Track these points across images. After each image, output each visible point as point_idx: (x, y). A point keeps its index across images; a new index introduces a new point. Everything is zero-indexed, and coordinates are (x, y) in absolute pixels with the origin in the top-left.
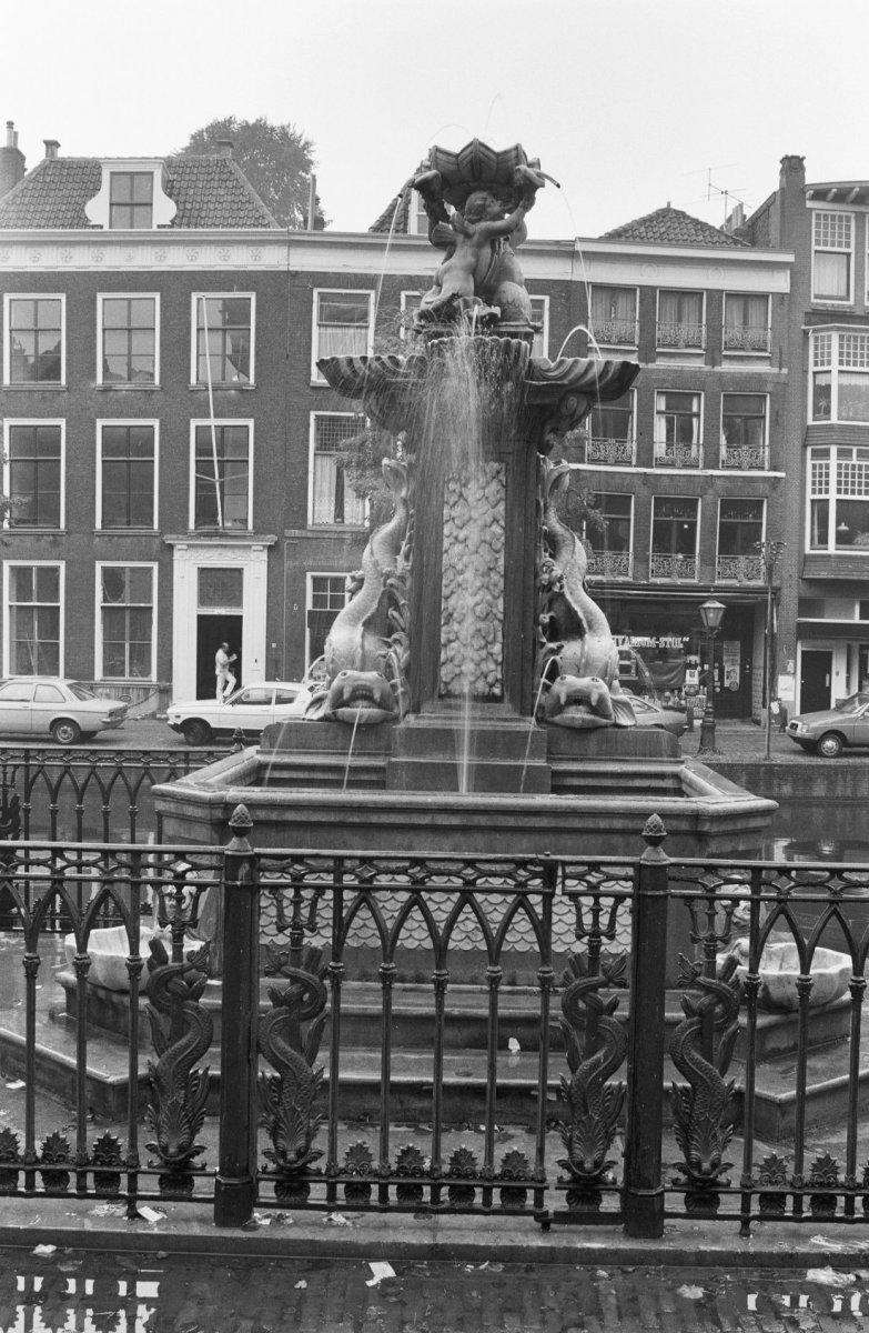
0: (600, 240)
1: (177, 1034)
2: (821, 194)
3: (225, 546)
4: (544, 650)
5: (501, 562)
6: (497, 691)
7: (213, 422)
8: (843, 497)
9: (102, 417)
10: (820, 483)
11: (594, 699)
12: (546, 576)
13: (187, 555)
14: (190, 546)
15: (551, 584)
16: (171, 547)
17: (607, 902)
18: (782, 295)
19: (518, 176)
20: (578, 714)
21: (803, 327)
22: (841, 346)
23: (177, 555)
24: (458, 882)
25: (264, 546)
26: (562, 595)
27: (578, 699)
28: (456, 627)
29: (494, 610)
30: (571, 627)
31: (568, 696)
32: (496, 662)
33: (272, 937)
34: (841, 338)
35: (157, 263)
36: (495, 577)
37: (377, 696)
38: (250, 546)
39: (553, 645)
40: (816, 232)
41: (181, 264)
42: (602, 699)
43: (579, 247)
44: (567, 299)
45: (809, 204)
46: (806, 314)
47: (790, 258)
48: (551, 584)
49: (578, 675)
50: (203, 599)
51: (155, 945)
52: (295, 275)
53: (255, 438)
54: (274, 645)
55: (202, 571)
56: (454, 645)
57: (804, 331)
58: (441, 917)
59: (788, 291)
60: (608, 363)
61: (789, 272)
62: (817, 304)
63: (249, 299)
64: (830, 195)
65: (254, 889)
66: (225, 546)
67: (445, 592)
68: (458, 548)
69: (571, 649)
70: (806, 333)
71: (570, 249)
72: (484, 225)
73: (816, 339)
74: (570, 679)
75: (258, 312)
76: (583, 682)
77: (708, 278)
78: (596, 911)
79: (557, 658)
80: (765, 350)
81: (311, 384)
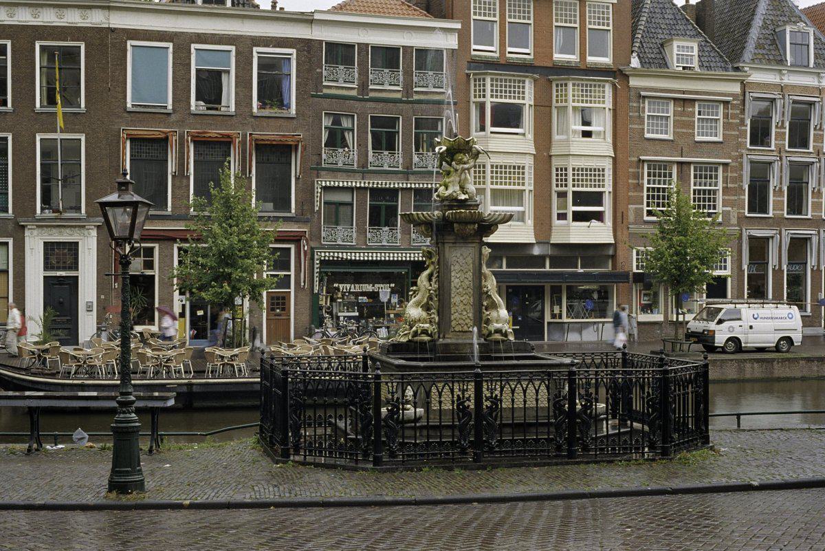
0: (328, 12)
1: (463, 417)
3: (64, 226)
4: (485, 315)
5: (472, 284)
7: (58, 136)
8: (495, 187)
10: (479, 178)
11: (504, 331)
12: (485, 289)
13: (35, 232)
14: (38, 226)
15: (487, 292)
16: (23, 227)
17: (395, 384)
18: (453, 50)
19: (474, 149)
20: (498, 337)
21: (467, 71)
22: (492, 85)
23: (27, 233)
24: (600, 357)
25: (94, 226)
26: (490, 296)
27: (498, 331)
28: (457, 308)
30: (494, 306)
31: (495, 330)
32: (471, 320)
33: (486, 393)
34: (492, 80)
35: (8, 19)
36: (470, 290)
37: (430, 332)
38: (85, 226)
39: (488, 313)
40: (474, 6)
41: (28, 19)
42: (506, 331)
43: (317, 17)
44: (309, 52)
46: (468, 62)
47: (459, 26)
48: (487, 292)
49: (67, 354)
50: (47, 266)
51: (458, 396)
52: (113, 30)
53: (86, 148)
54: (103, 297)
55: (45, 243)
56: (457, 314)
57: (467, 74)
58: (513, 386)
59: (457, 48)
60: (505, 215)
61: (457, 34)
62: (476, 56)
63: (80, 47)
65: (482, 381)
66: (64, 226)
67: (453, 295)
68: (457, 280)
69: (494, 314)
70: (468, 75)
71: (311, 18)
72: (461, 166)
73: (475, 80)
74: (495, 324)
75: (86, 57)
76: (499, 326)
77: (404, 38)
78: (393, 387)
79: (489, 317)
80: (442, 88)
81: (128, 110)
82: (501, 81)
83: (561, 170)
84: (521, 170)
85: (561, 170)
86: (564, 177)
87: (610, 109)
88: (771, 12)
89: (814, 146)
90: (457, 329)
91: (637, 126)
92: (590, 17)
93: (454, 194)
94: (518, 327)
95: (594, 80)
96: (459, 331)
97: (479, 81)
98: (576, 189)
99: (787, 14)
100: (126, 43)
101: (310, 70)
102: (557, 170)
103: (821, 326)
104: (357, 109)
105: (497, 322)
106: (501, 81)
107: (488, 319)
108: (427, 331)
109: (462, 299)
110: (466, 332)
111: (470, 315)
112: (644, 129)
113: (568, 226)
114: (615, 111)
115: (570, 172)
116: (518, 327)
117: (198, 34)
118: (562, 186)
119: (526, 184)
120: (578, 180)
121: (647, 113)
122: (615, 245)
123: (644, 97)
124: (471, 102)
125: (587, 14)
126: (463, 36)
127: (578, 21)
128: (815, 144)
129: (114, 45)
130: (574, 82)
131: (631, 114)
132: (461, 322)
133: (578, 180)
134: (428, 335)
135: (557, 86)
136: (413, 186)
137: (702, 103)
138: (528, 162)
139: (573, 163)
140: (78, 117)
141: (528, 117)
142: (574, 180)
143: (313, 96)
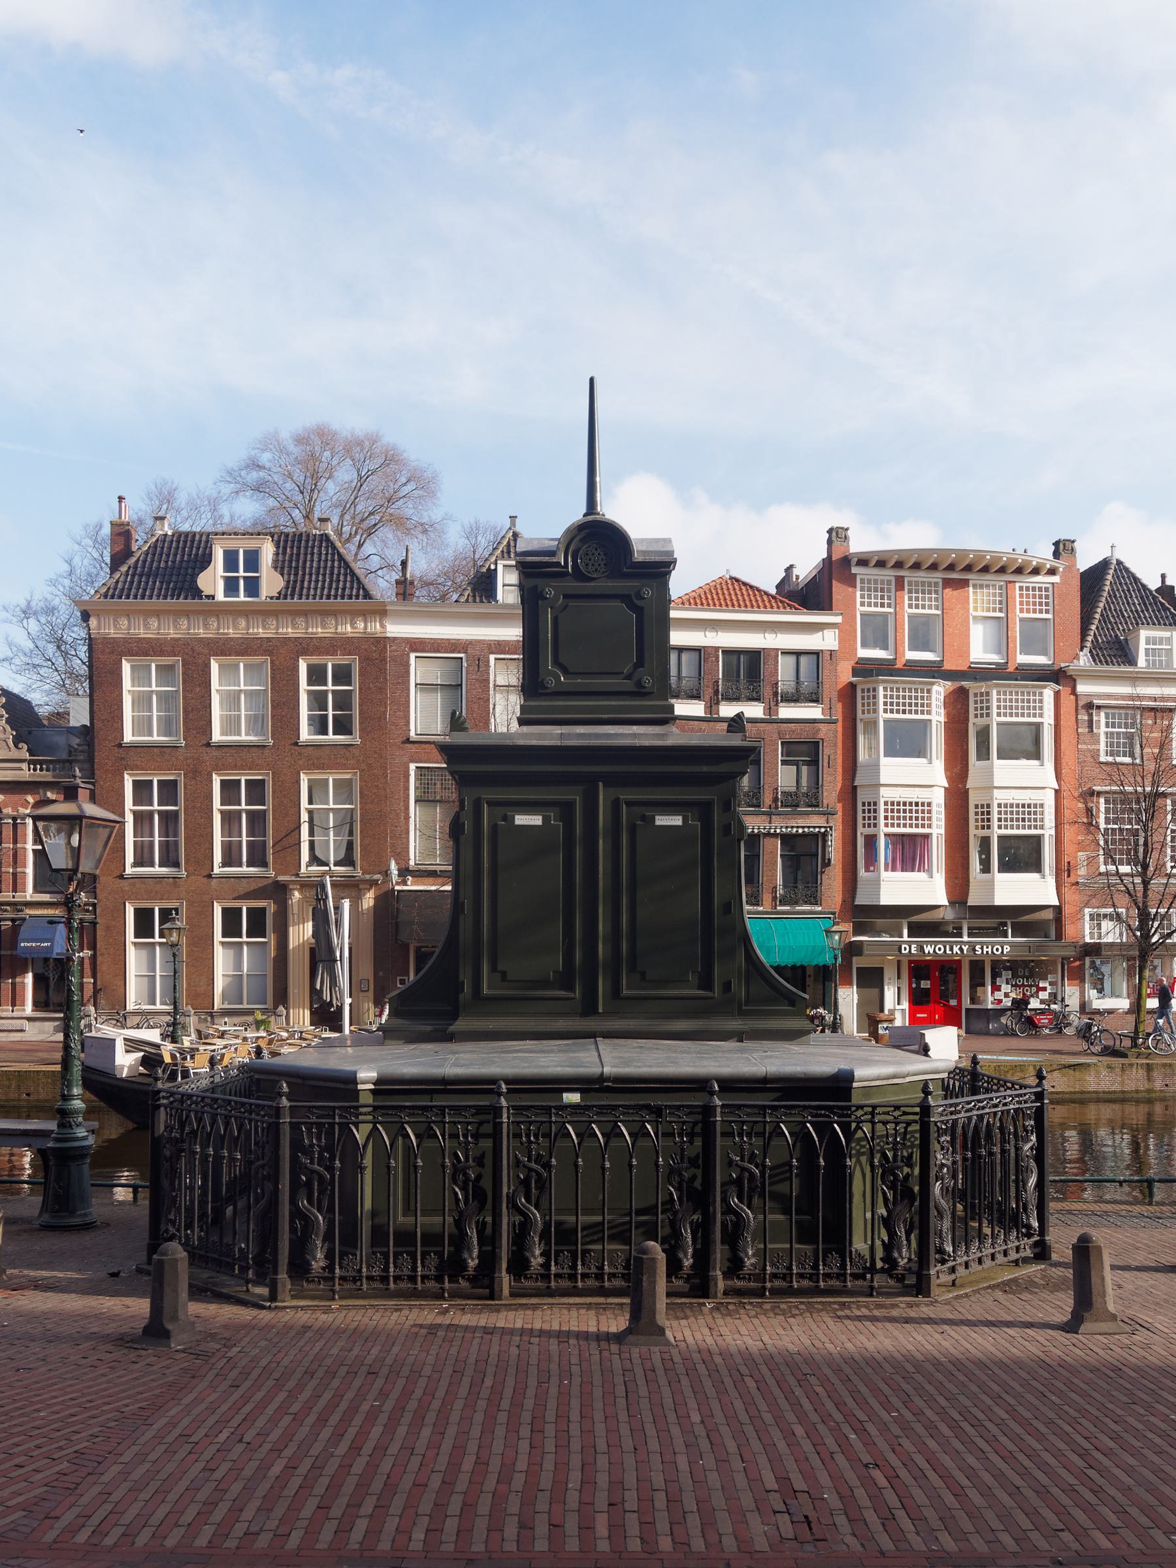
2: (863, 562)
9: (218, 768)
45: (854, 570)
64: (873, 563)
82: (916, 690)
83: (869, 804)
84: (926, 808)
85: (869, 804)
86: (890, 814)
92: (1021, 603)
94: (925, 1015)
95: (914, 683)
97: (869, 691)
98: (1004, 832)
100: (408, 655)
102: (864, 804)
106: (916, 690)
113: (992, 881)
115: (995, 809)
116: (925, 1015)
117: (498, 641)
118: (869, 826)
119: (934, 826)
120: (1006, 820)
122: (1058, 910)
123: (1099, 707)
124: (858, 721)
125: (1018, 599)
126: (846, 637)
127: (1051, 611)
129: (393, 659)
130: (885, 685)
133: (1006, 820)
135: (863, 691)
136: (778, 831)
137: (1110, 711)
138: (938, 798)
139: (999, 796)
140: (350, 749)
141: (937, 740)
142: (1000, 820)
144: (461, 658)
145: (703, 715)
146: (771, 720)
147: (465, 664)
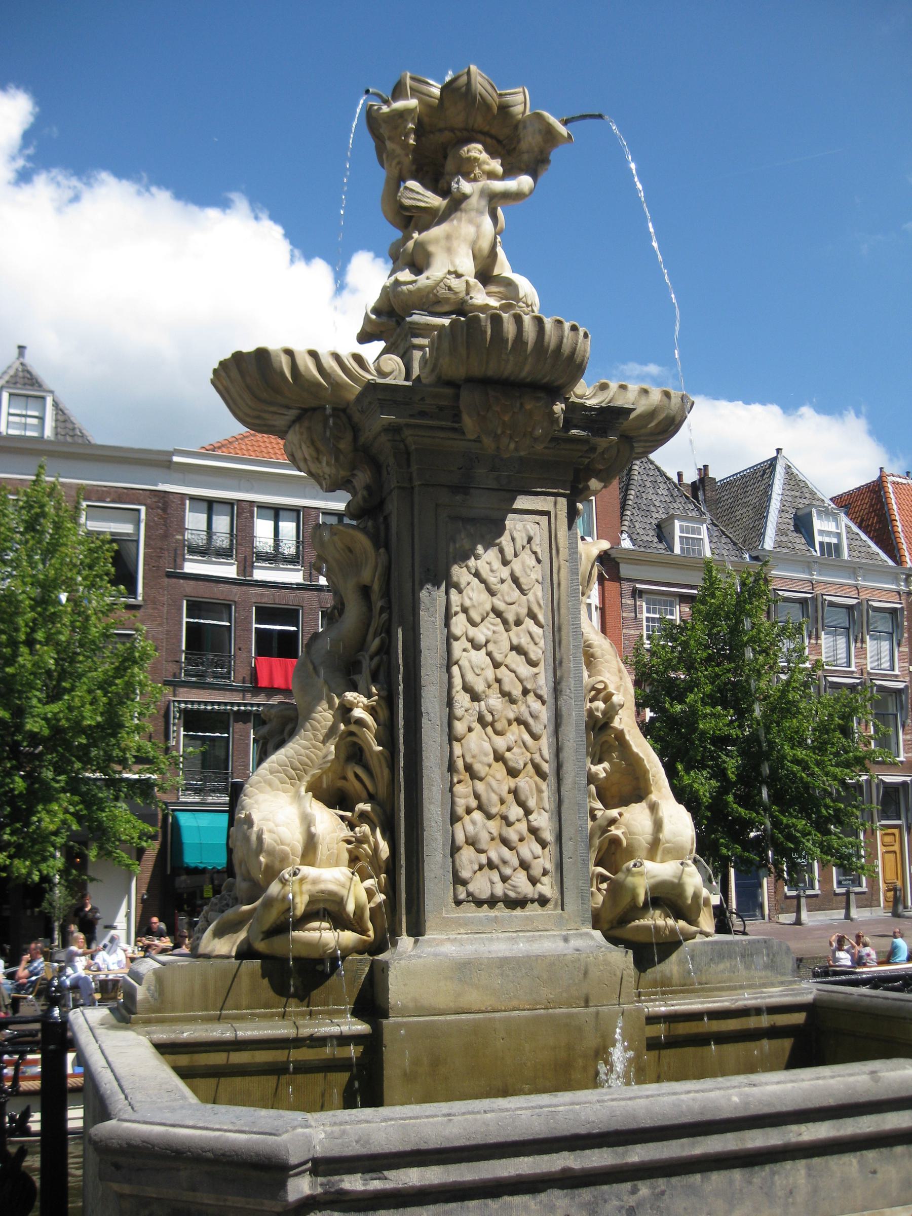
6: (547, 887)
29: (537, 757)
32: (543, 844)
37: (351, 907)
39: (614, 813)
44: (164, 510)
74: (648, 865)
87: (596, 608)
88: (788, 493)
89: (856, 663)
90: (481, 885)
91: (632, 632)
93: (454, 282)
96: (492, 902)
99: (807, 495)
101: (165, 536)
103: (879, 906)
104: (236, 595)
105: (667, 842)
107: (615, 841)
108: (340, 902)
109: (501, 743)
110: (520, 903)
111: (543, 820)
112: (642, 636)
114: (603, 610)
121: (645, 615)
128: (858, 661)
131: (624, 614)
132: (496, 852)
134: (339, 921)
143: (170, 575)
144: (138, 511)
145: (235, 576)
146: (244, 582)
147: (143, 516)
